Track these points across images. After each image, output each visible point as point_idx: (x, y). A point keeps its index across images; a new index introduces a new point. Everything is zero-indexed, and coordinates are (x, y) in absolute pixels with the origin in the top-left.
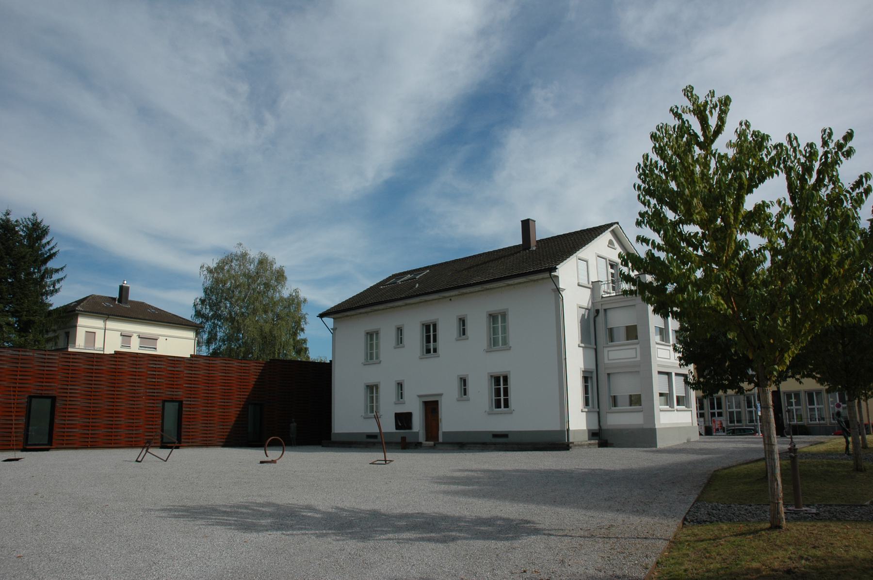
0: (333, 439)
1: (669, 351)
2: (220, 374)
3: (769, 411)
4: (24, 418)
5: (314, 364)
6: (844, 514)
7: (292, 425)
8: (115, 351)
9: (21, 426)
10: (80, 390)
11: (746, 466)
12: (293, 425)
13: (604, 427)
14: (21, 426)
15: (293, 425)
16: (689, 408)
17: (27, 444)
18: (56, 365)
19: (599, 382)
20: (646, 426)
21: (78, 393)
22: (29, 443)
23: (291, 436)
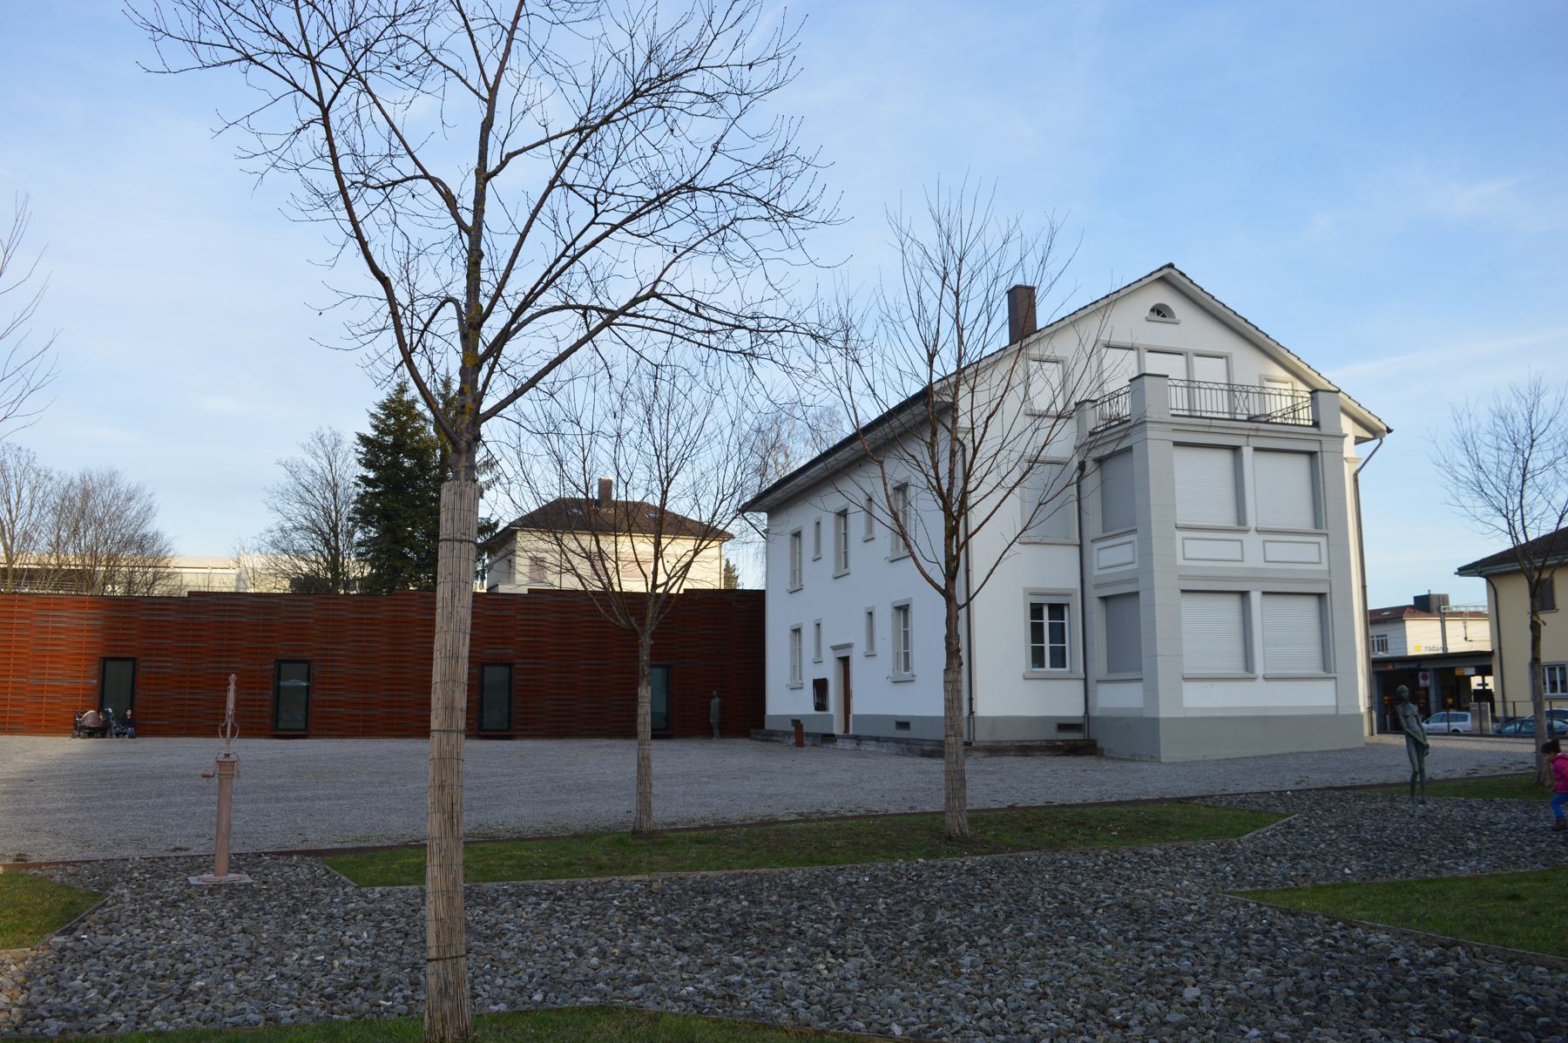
0: (769, 726)
1: (1317, 546)
2: (585, 619)
3: (226, 691)
4: (270, 692)
5: (203, 601)
6: (38, 1021)
7: (713, 701)
8: (1416, 598)
9: (267, 703)
10: (345, 650)
11: (1118, 809)
12: (716, 702)
13: (1094, 713)
14: (267, 703)
15: (716, 702)
16: (1330, 672)
17: (277, 729)
18: (310, 615)
19: (1087, 617)
20: (1148, 714)
21: (342, 655)
22: (281, 725)
23: (712, 720)
